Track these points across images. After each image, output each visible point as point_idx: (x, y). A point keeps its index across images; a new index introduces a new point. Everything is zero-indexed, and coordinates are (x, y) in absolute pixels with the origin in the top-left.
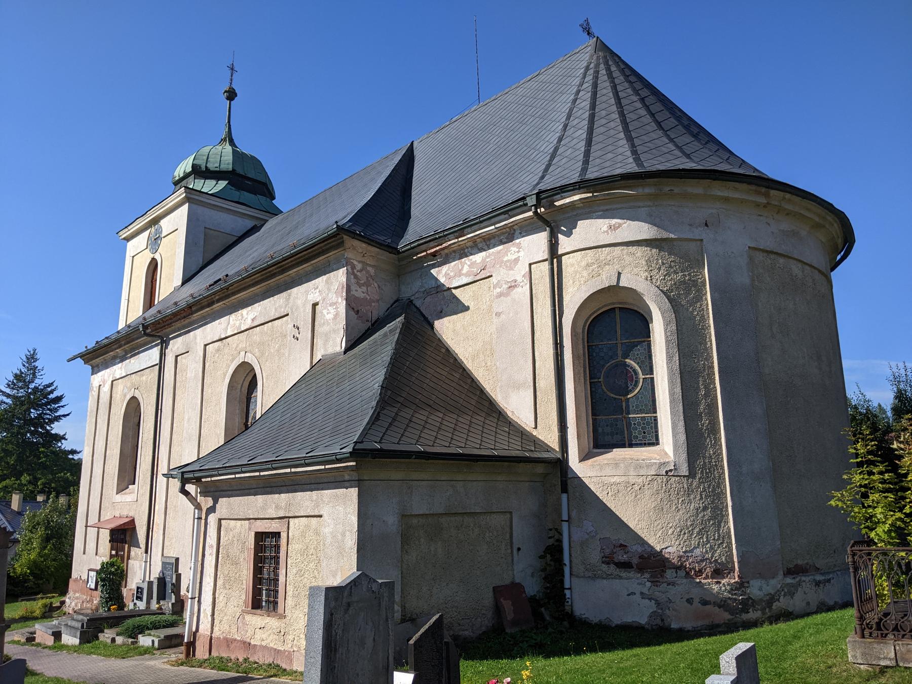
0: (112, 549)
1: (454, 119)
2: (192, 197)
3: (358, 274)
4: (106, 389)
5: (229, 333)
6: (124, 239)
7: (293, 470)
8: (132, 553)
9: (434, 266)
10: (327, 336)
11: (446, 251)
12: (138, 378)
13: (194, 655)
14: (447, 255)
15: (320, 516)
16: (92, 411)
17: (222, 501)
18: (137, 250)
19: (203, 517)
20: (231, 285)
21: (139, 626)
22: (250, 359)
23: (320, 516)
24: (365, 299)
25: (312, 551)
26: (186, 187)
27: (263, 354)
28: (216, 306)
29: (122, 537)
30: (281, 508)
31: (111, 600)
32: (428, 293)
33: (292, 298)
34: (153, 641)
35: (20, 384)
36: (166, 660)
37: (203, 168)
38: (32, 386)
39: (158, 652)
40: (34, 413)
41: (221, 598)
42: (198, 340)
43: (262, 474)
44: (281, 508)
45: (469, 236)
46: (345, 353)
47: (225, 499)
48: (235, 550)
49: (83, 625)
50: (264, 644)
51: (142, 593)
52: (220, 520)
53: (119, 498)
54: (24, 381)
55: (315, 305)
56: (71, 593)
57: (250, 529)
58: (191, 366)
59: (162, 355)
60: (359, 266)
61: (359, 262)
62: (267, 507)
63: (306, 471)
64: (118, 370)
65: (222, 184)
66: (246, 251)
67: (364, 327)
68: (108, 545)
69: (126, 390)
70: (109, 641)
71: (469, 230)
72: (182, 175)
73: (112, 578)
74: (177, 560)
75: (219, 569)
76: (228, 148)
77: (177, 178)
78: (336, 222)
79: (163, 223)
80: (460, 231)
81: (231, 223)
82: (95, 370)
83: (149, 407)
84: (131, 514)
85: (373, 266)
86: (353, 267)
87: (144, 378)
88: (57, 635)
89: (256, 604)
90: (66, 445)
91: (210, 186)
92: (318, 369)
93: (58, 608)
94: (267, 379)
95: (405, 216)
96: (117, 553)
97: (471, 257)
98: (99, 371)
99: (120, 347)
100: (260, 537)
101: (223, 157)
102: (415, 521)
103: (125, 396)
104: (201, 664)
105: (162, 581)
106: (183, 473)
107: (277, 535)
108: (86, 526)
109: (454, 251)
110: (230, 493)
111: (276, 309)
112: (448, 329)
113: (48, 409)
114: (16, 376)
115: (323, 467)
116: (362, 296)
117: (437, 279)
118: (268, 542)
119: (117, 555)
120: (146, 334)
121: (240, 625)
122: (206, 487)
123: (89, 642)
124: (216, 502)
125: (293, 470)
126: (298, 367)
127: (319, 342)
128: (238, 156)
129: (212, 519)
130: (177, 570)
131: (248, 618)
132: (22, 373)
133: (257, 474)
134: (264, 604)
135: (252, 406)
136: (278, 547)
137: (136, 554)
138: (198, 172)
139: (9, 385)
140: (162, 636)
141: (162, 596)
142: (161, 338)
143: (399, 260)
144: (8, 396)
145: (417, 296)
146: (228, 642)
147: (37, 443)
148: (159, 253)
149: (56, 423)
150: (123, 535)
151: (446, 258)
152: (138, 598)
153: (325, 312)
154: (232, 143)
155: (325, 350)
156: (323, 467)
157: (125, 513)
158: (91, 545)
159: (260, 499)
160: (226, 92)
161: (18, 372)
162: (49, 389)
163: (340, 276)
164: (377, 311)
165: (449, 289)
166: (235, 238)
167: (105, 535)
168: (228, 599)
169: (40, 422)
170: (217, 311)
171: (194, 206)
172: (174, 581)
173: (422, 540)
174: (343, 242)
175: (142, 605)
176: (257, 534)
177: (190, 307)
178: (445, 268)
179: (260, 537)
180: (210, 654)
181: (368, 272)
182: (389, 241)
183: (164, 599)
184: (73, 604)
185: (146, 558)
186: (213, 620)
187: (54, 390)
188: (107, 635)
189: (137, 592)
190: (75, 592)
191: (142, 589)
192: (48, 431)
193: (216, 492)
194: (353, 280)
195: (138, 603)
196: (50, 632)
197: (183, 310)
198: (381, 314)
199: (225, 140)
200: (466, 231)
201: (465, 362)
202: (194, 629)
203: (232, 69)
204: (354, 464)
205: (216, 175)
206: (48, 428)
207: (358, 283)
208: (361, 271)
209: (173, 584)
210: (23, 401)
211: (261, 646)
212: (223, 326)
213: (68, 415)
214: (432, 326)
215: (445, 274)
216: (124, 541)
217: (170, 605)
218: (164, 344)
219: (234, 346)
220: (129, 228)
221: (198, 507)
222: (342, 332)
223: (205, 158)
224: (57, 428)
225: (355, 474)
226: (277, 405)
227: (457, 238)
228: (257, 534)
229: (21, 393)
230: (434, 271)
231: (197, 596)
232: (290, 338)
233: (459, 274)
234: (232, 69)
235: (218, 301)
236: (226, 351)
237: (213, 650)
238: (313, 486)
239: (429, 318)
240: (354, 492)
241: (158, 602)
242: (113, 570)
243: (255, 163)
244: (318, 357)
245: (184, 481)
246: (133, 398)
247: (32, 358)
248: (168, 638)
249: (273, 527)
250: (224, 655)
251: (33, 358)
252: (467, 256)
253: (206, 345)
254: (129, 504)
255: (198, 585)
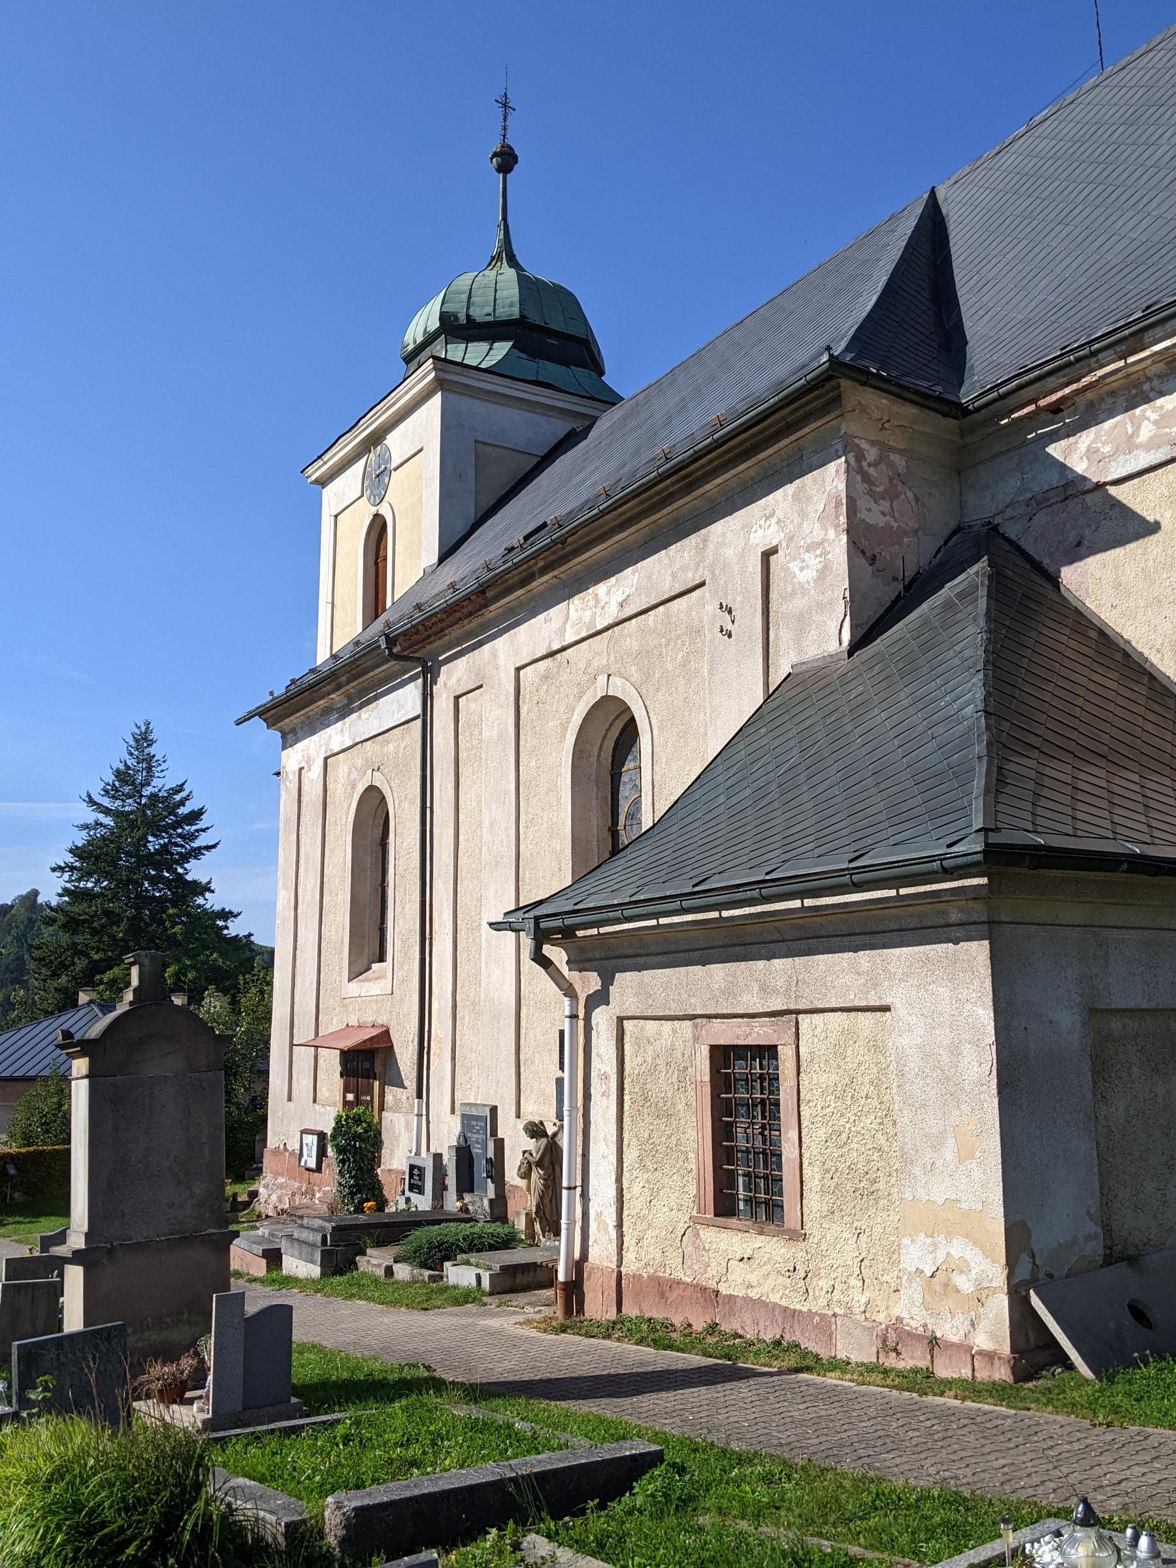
0: (346, 1090)
1: (1038, 118)
2: (450, 381)
3: (871, 470)
4: (314, 774)
5: (570, 638)
6: (316, 482)
7: (808, 902)
8: (389, 1098)
9: (1054, 437)
10: (802, 621)
11: (1090, 395)
12: (377, 748)
13: (581, 1310)
14: (1091, 405)
15: (886, 1009)
16: (287, 821)
17: (625, 981)
18: (344, 502)
19: (581, 1014)
20: (573, 532)
21: (441, 1244)
22: (620, 688)
23: (886, 1009)
24: (887, 528)
25: (867, 1088)
26: (435, 358)
27: (648, 676)
28: (539, 583)
29: (367, 1065)
30: (775, 991)
31: (359, 1191)
32: (1040, 502)
33: (711, 546)
34: (479, 1277)
35: (127, 789)
36: (521, 1318)
37: (462, 319)
38: (147, 791)
39: (493, 1301)
40: (153, 844)
41: (637, 1189)
42: (502, 659)
43: (725, 914)
44: (775, 991)
45: (1157, 348)
46: (851, 652)
47: (628, 975)
48: (663, 1085)
49: (324, 1238)
50: (754, 1294)
51: (421, 1177)
52: (620, 1020)
53: (353, 989)
54: (133, 784)
55: (768, 555)
56: (267, 1177)
57: (696, 1039)
58: (490, 715)
59: (427, 697)
60: (872, 453)
61: (873, 443)
62: (741, 992)
63: (846, 904)
64: (336, 735)
65: (502, 349)
66: (570, 479)
67: (888, 593)
68: (338, 1082)
69: (354, 775)
70: (380, 1272)
71: (1159, 331)
72: (420, 339)
73: (356, 1144)
74: (494, 1110)
75: (626, 1126)
76: (510, 274)
77: (411, 347)
78: (828, 348)
79: (393, 440)
80: (1131, 339)
81: (526, 429)
82: (289, 738)
83: (406, 805)
84: (382, 1020)
85: (902, 452)
86: (860, 457)
87: (391, 747)
88: (273, 1258)
89: (725, 1207)
90: (212, 902)
91: (481, 354)
92: (787, 701)
93: (247, 1204)
94: (661, 728)
95: (951, 342)
96: (357, 1097)
97: (1160, 402)
98: (297, 741)
99: (338, 687)
100: (722, 1056)
101: (499, 291)
102: (1116, 1025)
103: (354, 786)
104: (608, 1330)
105: (464, 1154)
106: (537, 919)
107: (770, 1052)
108: (292, 1045)
109: (1112, 394)
110: (642, 960)
111: (674, 576)
112: (1100, 584)
113: (179, 836)
114: (118, 774)
115: (893, 893)
116: (882, 521)
117: (1063, 467)
118: (739, 1068)
119: (357, 1102)
120: (397, 657)
121: (689, 1250)
122: (582, 950)
123: (341, 1273)
124: (607, 980)
125: (808, 902)
126: (735, 700)
127: (781, 635)
128: (527, 284)
129: (602, 1018)
130: (494, 1133)
131: (708, 1235)
132: (128, 768)
133: (714, 915)
134: (741, 1206)
135: (625, 791)
136: (771, 1081)
137: (398, 1102)
138: (454, 327)
139: (107, 791)
140: (497, 1267)
141: (466, 1184)
142: (422, 662)
143: (963, 433)
144: (107, 811)
145: (1009, 513)
146: (663, 1287)
147: (161, 901)
148: (392, 497)
149: (193, 861)
150: (367, 1063)
151: (1088, 413)
152: (412, 1188)
153: (794, 567)
154: (513, 261)
155: (800, 651)
156: (893, 893)
157: (369, 1018)
158: (303, 1084)
159: (718, 972)
160: (495, 155)
161: (122, 767)
162: (178, 797)
163: (830, 480)
164: (914, 555)
165: (1100, 486)
166: (535, 460)
167: (331, 1062)
168: (654, 1194)
169: (166, 859)
170: (541, 594)
171: (454, 398)
172: (491, 1154)
173: (1135, 1069)
174: (839, 397)
175: (423, 1203)
176: (714, 1049)
177: (482, 591)
178: (1086, 439)
179: (722, 1056)
180: (619, 1310)
181: (891, 465)
182: (939, 388)
183: (471, 1190)
184: (274, 1198)
185: (420, 1108)
186: (621, 1236)
187: (187, 798)
188: (374, 1261)
189: (411, 1176)
190: (276, 1174)
191: (421, 1170)
192: (180, 876)
193: (609, 960)
194: (861, 487)
195: (415, 1198)
196: (259, 1250)
197: (467, 598)
198: (924, 562)
199: (498, 257)
200: (1148, 336)
201: (1154, 658)
202: (577, 1255)
203: (505, 105)
204: (983, 881)
205: (488, 331)
206: (180, 870)
207: (871, 493)
208: (875, 464)
209: (489, 1161)
210: (133, 821)
211: (747, 1299)
212: (555, 625)
213: (214, 846)
214: (1054, 581)
215: (1082, 453)
216: (370, 1075)
217: (486, 1203)
218: (430, 674)
219: (582, 665)
220: (326, 457)
221: (569, 991)
222: (840, 608)
223: (465, 297)
224: (195, 871)
225: (978, 906)
226: (709, 775)
227: (1124, 357)
228: (714, 1049)
229: (130, 806)
230: (1055, 450)
231: (579, 1183)
232: (711, 634)
233: (1129, 445)
234: (505, 105)
235: (543, 571)
236: (565, 676)
237: (625, 1302)
238: (858, 940)
239: (1046, 562)
240: (978, 952)
241: (460, 1197)
242: (360, 1130)
243: (565, 299)
244: (782, 669)
245: (541, 937)
246: (372, 790)
247: (144, 739)
248: (510, 1271)
249: (757, 1034)
250: (657, 1315)
251: (145, 739)
252: (1148, 400)
253: (518, 669)
254: (377, 1001)
255: (579, 1159)
